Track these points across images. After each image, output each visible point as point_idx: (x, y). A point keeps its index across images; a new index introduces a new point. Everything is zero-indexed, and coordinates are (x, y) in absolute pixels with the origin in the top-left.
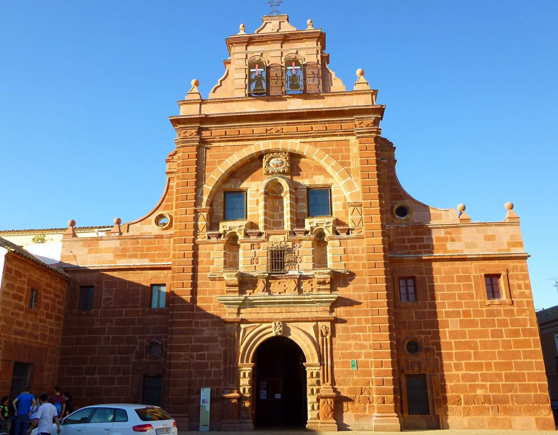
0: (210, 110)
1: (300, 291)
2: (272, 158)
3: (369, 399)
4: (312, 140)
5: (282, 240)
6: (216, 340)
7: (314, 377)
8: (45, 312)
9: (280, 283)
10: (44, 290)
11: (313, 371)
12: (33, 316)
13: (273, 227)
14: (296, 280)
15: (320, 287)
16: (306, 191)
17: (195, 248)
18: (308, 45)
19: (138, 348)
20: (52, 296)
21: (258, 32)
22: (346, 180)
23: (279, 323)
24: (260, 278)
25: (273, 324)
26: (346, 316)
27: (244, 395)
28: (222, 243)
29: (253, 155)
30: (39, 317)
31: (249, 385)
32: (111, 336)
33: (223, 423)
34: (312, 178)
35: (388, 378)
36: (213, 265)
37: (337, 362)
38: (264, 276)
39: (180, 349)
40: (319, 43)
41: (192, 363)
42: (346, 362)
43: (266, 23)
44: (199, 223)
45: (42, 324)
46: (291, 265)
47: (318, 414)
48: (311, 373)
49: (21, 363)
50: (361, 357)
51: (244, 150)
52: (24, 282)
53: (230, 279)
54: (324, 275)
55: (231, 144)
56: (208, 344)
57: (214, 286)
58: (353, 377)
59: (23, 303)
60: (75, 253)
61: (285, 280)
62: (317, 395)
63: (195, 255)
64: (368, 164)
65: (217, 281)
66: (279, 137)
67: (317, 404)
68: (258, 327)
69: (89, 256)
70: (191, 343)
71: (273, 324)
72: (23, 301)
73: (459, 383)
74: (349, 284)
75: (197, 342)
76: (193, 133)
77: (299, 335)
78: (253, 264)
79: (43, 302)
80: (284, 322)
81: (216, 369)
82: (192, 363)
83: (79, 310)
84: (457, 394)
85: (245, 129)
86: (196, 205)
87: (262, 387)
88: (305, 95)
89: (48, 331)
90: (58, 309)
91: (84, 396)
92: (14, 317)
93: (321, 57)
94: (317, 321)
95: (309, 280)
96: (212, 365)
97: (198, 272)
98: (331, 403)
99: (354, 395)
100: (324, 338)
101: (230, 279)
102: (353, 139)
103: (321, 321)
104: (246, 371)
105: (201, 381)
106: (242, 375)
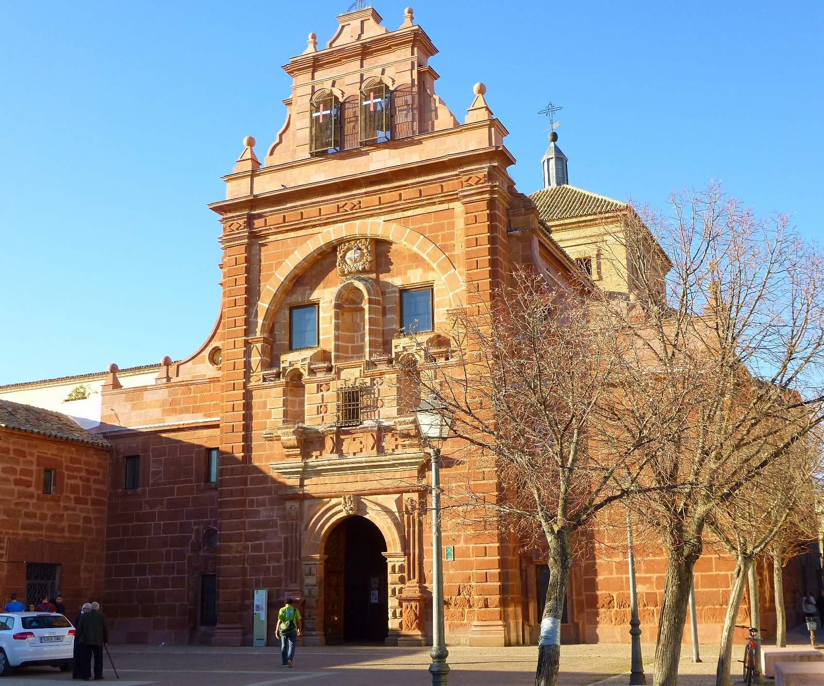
0: (266, 186)
1: (381, 450)
2: (349, 249)
3: (469, 601)
4: (400, 215)
5: (358, 375)
6: (275, 524)
8: (72, 496)
9: (354, 439)
10: (68, 468)
12: (52, 503)
13: (352, 355)
16: (398, 295)
17: (248, 396)
18: (398, 57)
19: (193, 538)
20: (83, 474)
21: (331, 44)
22: (447, 274)
23: (350, 498)
28: (279, 386)
29: (322, 248)
30: (62, 504)
32: (162, 523)
34: (406, 274)
35: (492, 571)
39: (230, 538)
40: (416, 49)
41: (246, 556)
43: (343, 27)
44: (253, 359)
45: (70, 512)
47: (401, 624)
49: (36, 565)
50: (459, 542)
51: (308, 242)
52: (32, 462)
54: (406, 426)
55: (292, 234)
56: (265, 530)
57: (272, 448)
58: (448, 571)
59: (32, 489)
60: (116, 411)
61: (361, 435)
63: (248, 407)
64: (477, 246)
66: (354, 217)
69: (133, 413)
70: (245, 530)
72: (31, 486)
73: (612, 576)
75: (253, 528)
76: (241, 225)
79: (67, 483)
80: (357, 498)
82: (246, 556)
83: (125, 489)
84: (608, 592)
85: (309, 208)
86: (247, 333)
87: (373, 586)
88: (393, 143)
89: (82, 521)
90: (94, 489)
91: (135, 603)
92: (20, 508)
93: (419, 73)
94: (401, 492)
96: (271, 558)
97: (252, 431)
98: (416, 607)
99: (449, 597)
102: (458, 206)
103: (406, 492)
105: (258, 581)
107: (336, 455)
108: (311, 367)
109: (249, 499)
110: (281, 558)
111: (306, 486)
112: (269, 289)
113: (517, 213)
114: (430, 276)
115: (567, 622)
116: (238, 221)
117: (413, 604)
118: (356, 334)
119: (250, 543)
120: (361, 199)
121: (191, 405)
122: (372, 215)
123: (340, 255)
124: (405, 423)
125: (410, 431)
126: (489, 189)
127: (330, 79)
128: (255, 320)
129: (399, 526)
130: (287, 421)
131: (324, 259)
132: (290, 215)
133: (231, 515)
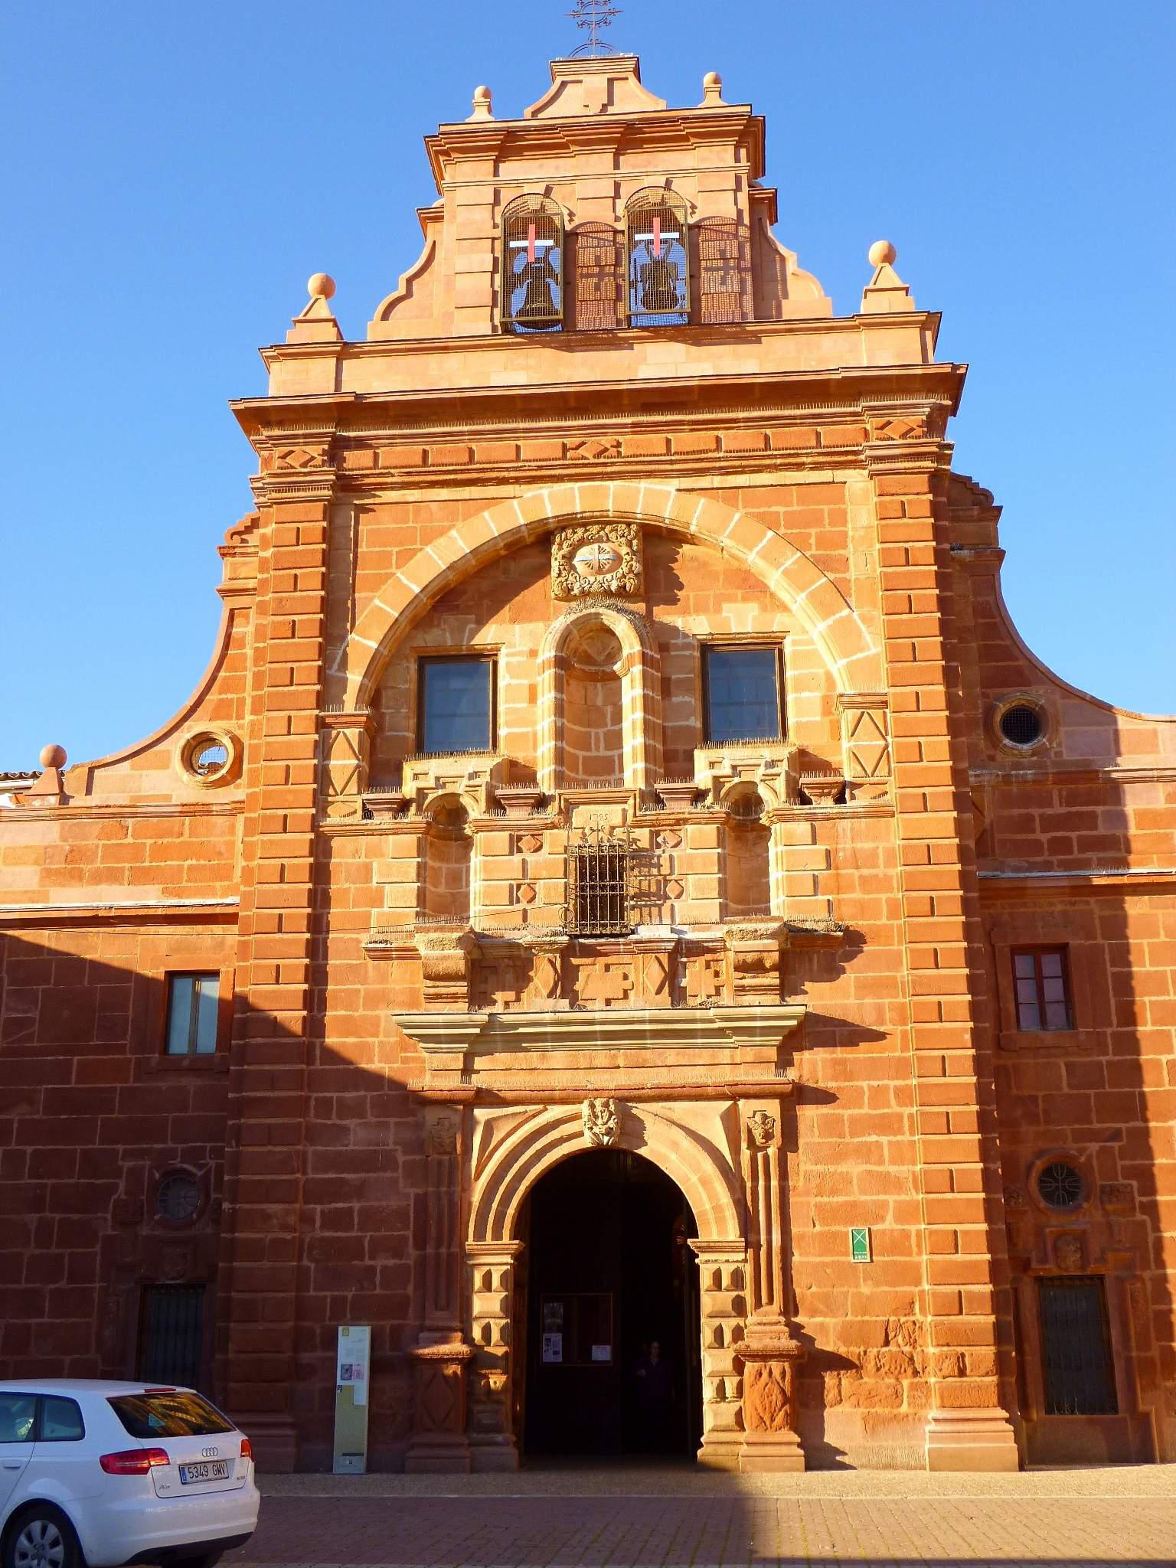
1: (678, 996)
2: (582, 543)
3: (911, 1359)
4: (717, 481)
5: (617, 820)
6: (389, 1162)
9: (607, 968)
14: (664, 958)
16: (697, 654)
17: (321, 847)
21: (535, 113)
23: (606, 1105)
26: (835, 1078)
27: (486, 1349)
31: (501, 1314)
32: (29, 1149)
33: (412, 1447)
34: (718, 610)
36: (381, 905)
37: (802, 1237)
38: (555, 943)
39: (267, 1192)
41: (307, 1240)
43: (564, 84)
44: (334, 763)
47: (739, 1414)
50: (882, 1219)
51: (486, 514)
53: (437, 953)
55: (444, 493)
57: (383, 978)
58: (857, 1286)
61: (627, 958)
65: (396, 962)
66: (607, 473)
68: (534, 1116)
70: (304, 1173)
71: (584, 1108)
76: (313, 458)
77: (675, 1146)
78: (518, 901)
80: (623, 1102)
81: (391, 1262)
82: (307, 1240)
86: (322, 701)
87: (549, 1321)
94: (735, 1097)
95: (708, 957)
97: (328, 932)
98: (783, 1373)
99: (862, 1349)
100: (760, 1155)
101: (437, 953)
102: (856, 480)
107: (565, 1004)
108: (498, 792)
109: (317, 1099)
111: (478, 1072)
112: (381, 608)
113: (961, 513)
114: (777, 623)
115: (1116, 1412)
116: (307, 448)
117: (776, 1366)
118: (593, 731)
119: (319, 1208)
120: (621, 439)
121: (127, 865)
122: (649, 474)
123: (562, 552)
124: (756, 935)
125: (765, 954)
126: (935, 449)
127: (539, 180)
128: (341, 674)
129: (731, 1177)
130: (424, 915)
131: (514, 559)
132: (439, 452)
133: (270, 1136)
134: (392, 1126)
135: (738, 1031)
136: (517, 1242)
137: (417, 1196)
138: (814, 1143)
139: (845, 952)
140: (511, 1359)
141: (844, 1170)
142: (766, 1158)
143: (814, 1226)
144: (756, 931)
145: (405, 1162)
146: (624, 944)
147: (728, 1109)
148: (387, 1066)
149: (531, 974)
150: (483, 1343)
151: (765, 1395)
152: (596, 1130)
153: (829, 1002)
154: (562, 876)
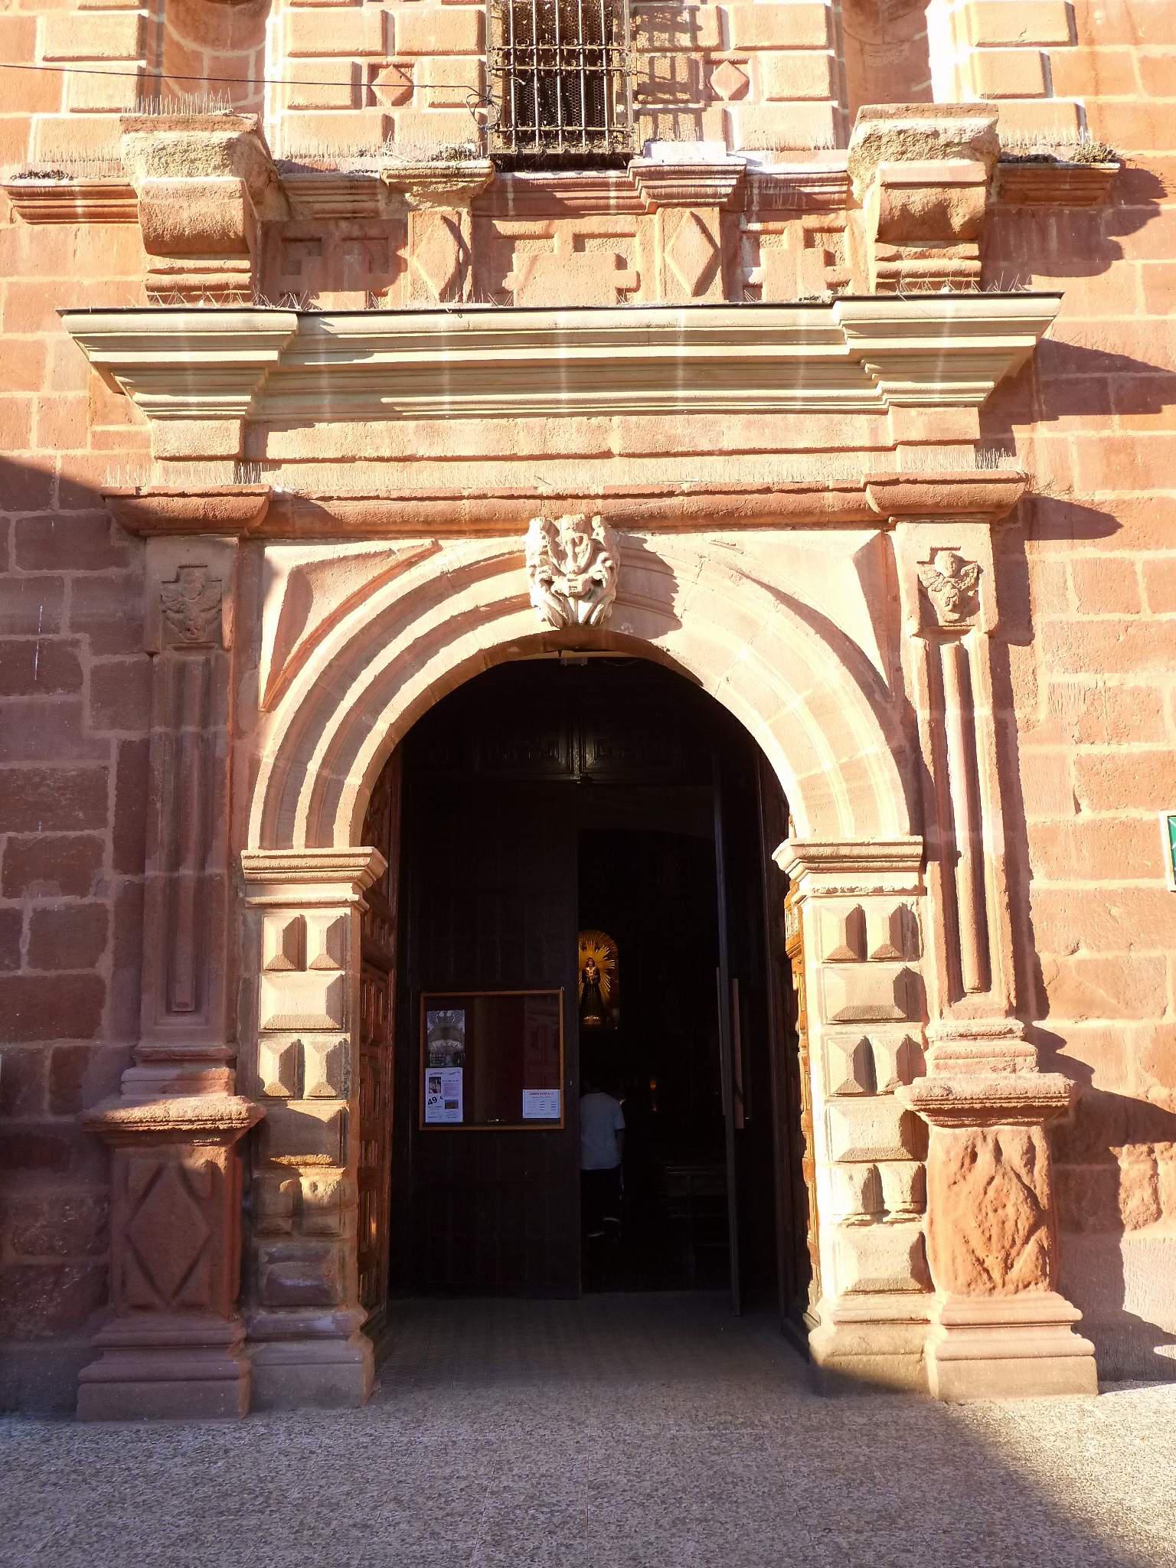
7: (872, 948)
9: (579, 242)
11: (869, 905)
14: (712, 217)
15: (905, 265)
23: (585, 527)
24: (424, 196)
25: (533, 541)
26: (1109, 481)
27: (294, 1105)
31: (329, 1023)
33: (98, 1352)
36: (54, 106)
37: (1051, 834)
38: (458, 174)
42: (1128, 828)
46: (665, 111)
47: (919, 1251)
48: (849, 919)
53: (177, 181)
54: (937, 163)
57: (55, 261)
61: (623, 223)
62: (901, 1091)
65: (85, 227)
67: (910, 1168)
68: (409, 564)
71: (533, 541)
74: (1117, 253)
77: (748, 626)
78: (373, 101)
81: (59, 902)
87: (436, 1045)
95: (811, 221)
98: (1031, 1150)
100: (947, 651)
101: (177, 181)
104: (308, 913)
106: (272, 946)
110: (99, 863)
111: (276, 464)
117: (1011, 1137)
125: (954, 194)
134: (68, 589)
135: (893, 363)
136: (368, 850)
137: (126, 747)
138: (1070, 625)
139: (1119, 214)
140: (354, 1125)
141: (1142, 684)
142: (962, 659)
143: (1078, 809)
144: (935, 134)
145: (96, 671)
146: (619, 186)
147: (870, 547)
148: (59, 453)
149: (403, 253)
150: (285, 1092)
151: (988, 1205)
152: (561, 585)
153: (1088, 319)
154: (471, 43)
